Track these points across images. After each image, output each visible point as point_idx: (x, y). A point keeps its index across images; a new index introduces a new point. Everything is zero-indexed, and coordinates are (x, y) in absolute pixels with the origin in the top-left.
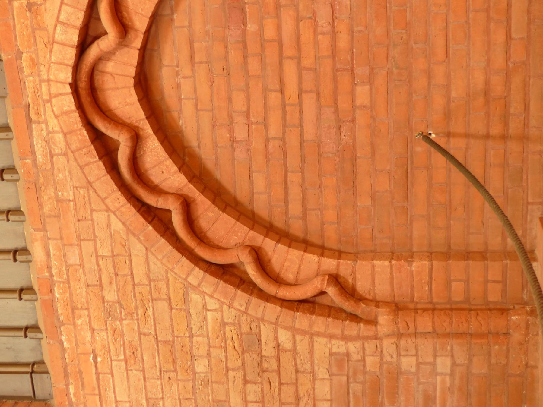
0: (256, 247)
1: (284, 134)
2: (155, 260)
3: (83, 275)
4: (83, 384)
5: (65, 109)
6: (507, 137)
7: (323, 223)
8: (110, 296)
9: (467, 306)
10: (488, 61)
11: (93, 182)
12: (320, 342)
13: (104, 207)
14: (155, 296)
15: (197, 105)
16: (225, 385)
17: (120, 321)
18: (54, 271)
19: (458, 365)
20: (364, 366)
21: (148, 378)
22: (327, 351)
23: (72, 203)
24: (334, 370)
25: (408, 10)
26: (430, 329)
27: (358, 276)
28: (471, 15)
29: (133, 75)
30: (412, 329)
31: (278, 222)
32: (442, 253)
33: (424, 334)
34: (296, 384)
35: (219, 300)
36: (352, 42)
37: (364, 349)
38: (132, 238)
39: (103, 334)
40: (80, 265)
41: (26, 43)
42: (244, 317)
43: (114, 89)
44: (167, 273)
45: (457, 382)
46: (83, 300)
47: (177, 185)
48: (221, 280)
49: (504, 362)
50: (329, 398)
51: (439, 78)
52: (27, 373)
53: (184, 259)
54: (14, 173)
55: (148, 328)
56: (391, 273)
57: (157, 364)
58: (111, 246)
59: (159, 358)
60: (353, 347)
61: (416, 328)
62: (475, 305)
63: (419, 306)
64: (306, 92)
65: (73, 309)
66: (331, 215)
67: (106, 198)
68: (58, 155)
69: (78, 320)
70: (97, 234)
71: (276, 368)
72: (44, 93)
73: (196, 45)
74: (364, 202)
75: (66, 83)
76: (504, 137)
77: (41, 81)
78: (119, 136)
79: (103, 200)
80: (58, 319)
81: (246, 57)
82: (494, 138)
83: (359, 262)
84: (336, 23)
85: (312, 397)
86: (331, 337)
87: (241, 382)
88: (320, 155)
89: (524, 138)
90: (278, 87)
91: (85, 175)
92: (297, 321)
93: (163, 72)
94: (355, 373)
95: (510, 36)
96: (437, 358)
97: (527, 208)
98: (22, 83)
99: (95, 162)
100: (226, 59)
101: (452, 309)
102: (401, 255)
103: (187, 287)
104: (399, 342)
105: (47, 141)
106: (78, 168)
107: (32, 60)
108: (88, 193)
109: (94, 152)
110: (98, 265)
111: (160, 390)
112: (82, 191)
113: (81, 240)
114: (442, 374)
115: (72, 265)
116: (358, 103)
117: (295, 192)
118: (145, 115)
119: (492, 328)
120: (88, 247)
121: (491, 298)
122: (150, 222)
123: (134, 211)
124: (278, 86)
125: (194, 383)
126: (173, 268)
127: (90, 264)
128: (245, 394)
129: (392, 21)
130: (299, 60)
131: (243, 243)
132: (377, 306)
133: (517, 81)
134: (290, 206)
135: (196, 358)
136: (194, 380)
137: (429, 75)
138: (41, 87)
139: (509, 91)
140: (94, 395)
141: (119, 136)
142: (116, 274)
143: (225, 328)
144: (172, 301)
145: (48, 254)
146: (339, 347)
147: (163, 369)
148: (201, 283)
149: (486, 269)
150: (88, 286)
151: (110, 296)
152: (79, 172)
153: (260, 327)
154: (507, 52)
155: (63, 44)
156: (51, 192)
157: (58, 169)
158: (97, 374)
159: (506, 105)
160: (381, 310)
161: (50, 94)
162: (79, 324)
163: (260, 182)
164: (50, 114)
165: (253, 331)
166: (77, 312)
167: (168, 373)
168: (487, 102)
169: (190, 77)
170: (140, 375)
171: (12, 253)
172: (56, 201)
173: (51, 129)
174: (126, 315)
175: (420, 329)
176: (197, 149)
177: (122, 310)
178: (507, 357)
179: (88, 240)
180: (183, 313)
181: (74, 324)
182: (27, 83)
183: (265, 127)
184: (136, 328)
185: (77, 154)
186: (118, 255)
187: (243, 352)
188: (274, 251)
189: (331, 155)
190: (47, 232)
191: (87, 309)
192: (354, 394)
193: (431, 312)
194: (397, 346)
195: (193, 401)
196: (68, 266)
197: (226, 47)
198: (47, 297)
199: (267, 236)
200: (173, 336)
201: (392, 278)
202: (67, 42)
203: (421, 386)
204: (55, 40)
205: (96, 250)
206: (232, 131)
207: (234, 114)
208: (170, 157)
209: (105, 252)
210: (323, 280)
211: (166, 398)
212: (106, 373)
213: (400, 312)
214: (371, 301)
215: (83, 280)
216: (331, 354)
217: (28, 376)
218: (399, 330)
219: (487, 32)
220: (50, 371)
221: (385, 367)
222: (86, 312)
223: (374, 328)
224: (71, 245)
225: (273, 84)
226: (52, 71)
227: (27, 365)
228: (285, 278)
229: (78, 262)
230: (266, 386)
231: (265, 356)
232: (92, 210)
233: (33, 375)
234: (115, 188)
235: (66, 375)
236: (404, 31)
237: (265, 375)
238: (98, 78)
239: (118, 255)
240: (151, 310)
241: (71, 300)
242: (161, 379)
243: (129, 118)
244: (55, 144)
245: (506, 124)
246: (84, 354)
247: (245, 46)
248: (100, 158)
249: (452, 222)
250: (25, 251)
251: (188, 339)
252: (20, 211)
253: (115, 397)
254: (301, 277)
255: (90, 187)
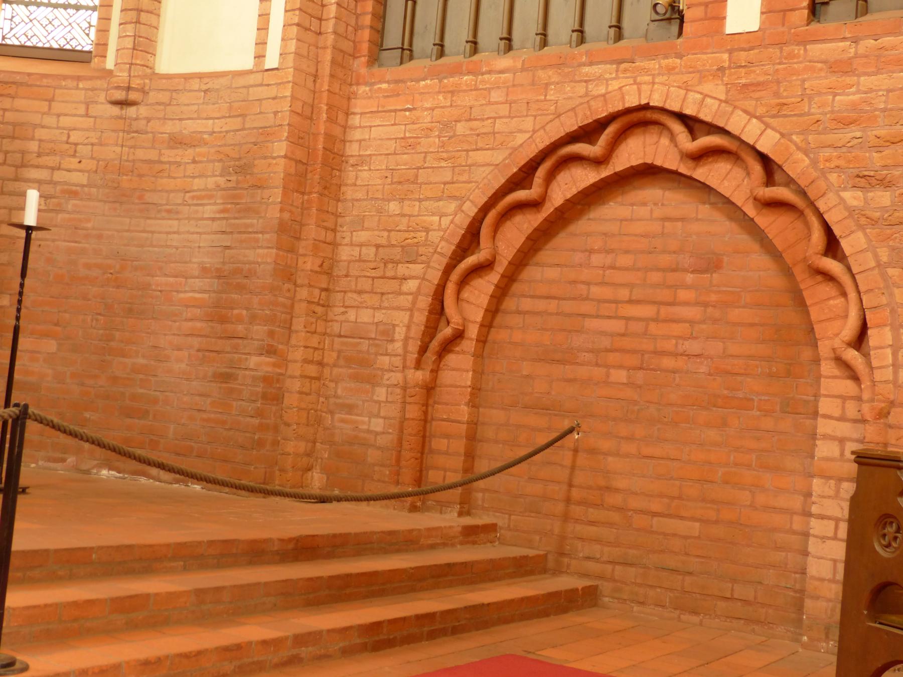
0: (494, 266)
1: (592, 300)
2: (487, 172)
3: (480, 103)
4: (388, 96)
5: (627, 97)
6: (568, 503)
7: (511, 328)
8: (461, 128)
9: (426, 451)
10: (636, 494)
11: (560, 119)
12: (404, 317)
13: (537, 127)
14: (457, 170)
15: (626, 220)
16: (377, 228)
17: (438, 135)
18: (486, 77)
19: (376, 437)
20: (382, 355)
21: (388, 158)
22: (396, 323)
23: (543, 98)
24: (381, 328)
25: (688, 425)
26: (407, 416)
27: (461, 356)
28: (677, 483)
29: (655, 163)
30: (409, 400)
31: (516, 287)
32: (476, 433)
33: (403, 410)
34: (372, 292)
35: (448, 228)
36: (666, 371)
37: (396, 355)
38: (508, 152)
39: (429, 119)
40: (489, 101)
41: (689, 64)
42: (432, 251)
43: (644, 142)
44: (476, 182)
45: (362, 435)
46: (459, 103)
47: (554, 196)
48: (465, 232)
49: (376, 477)
50: (358, 321)
51: (627, 447)
52: (403, 44)
53: (485, 199)
54: (577, 44)
55: (430, 161)
56: (460, 387)
57: (399, 167)
58: (503, 132)
59: (404, 169)
60: (398, 346)
61: (410, 403)
62: (427, 458)
63: (430, 409)
64: (627, 325)
65: (452, 92)
66: (518, 336)
67: (545, 130)
68: (587, 88)
69: (443, 96)
70: (515, 119)
71: (387, 275)
72: (642, 78)
73: (679, 224)
74: (526, 368)
75: (649, 99)
76: (568, 500)
77: (653, 75)
78: (600, 146)
79: (543, 127)
80: (445, 78)
81: (664, 270)
82: (569, 491)
83: (473, 358)
84: (684, 357)
85: (360, 305)
86: (408, 327)
87: (377, 242)
88: (570, 331)
89: (566, 518)
90: (634, 298)
91: (566, 112)
92: (424, 298)
93: (658, 191)
94: (377, 345)
95: (655, 516)
96: (383, 420)
97: (506, 514)
98: (654, 57)
99: (577, 123)
100: (664, 252)
101: (424, 437)
102: (477, 397)
103: (461, 199)
104: (399, 387)
105: (599, 78)
106: (573, 106)
107: (674, 68)
108: (551, 114)
109: (586, 122)
110: (488, 118)
111: (377, 168)
112: (553, 108)
113: (510, 104)
114: (370, 422)
115: (490, 94)
116: (612, 371)
117: (541, 305)
118: (618, 172)
119: (404, 470)
120: (504, 110)
121: (431, 472)
122: (520, 169)
123: (532, 156)
124: (634, 298)
125: (381, 200)
126: (479, 189)
127: (489, 111)
128: (368, 245)
129: (680, 409)
130: (656, 320)
131: (498, 253)
132: (432, 371)
133: (616, 517)
134: (529, 299)
135: (401, 204)
136: (383, 199)
137: (630, 438)
138: (649, 75)
139: (608, 510)
140: (378, 107)
141: (600, 146)
142: (478, 135)
143: (424, 232)
144: (451, 185)
145: (501, 72)
146: (400, 333)
147: (395, 172)
148: (464, 214)
149: (455, 471)
150: (471, 108)
151: (461, 128)
152: (569, 107)
153: (422, 263)
154: (642, 512)
155: (684, 100)
156: (555, 79)
157: (575, 86)
158: (395, 111)
159: (595, 505)
160: (428, 373)
161: (641, 84)
162: (439, 97)
163: (552, 273)
164: (624, 82)
165: (419, 257)
166: (450, 95)
167: (390, 177)
168: (600, 488)
169: (651, 216)
170: (391, 151)
171: (508, 36)
172: (547, 83)
173: (610, 82)
174: (443, 142)
175: (408, 407)
176: (587, 217)
177: (447, 138)
178: (379, 481)
179: (510, 111)
180: (440, 194)
181: (439, 92)
182: (653, 62)
183: (600, 283)
184: (431, 150)
185: (586, 105)
186: (495, 138)
187: (402, 246)
188: (489, 282)
189: (569, 341)
190: (521, 72)
191: (451, 105)
192: (360, 343)
193: (423, 418)
194: (396, 385)
195: (366, 197)
196: (489, 90)
197: (674, 252)
198: (464, 68)
199: (503, 276)
200: (421, 184)
201: (457, 387)
202: (685, 104)
203: (361, 403)
204: (689, 92)
205: (500, 117)
206: (599, 251)
207: (614, 255)
208: (579, 192)
209: (499, 125)
210: (458, 324)
211: (370, 173)
212: (395, 119)
213: (425, 391)
214: (438, 366)
215: (476, 103)
216: (394, 326)
217: (400, 46)
218: (409, 388)
219: (661, 495)
220: (403, 66)
221: (380, 373)
222: (449, 104)
223: (413, 366)
224: (507, 95)
225: (637, 294)
226: (661, 87)
227: (411, 44)
228: (465, 290)
229: (492, 100)
230: (372, 265)
231: (397, 266)
232: (535, 117)
233: (401, 50)
234: (553, 140)
235: (397, 82)
236: (670, 420)
237: (382, 265)
238: (654, 129)
239: (495, 138)
240: (445, 165)
241: (459, 91)
242: (387, 169)
243: (617, 156)
244: (597, 85)
245: (580, 503)
246: (413, 99)
247: (674, 270)
248: (580, 127)
249: (501, 445)
250: (509, 48)
251: (418, 197)
252: (544, 46)
253: (375, 126)
254: (465, 305)
255: (555, 116)
